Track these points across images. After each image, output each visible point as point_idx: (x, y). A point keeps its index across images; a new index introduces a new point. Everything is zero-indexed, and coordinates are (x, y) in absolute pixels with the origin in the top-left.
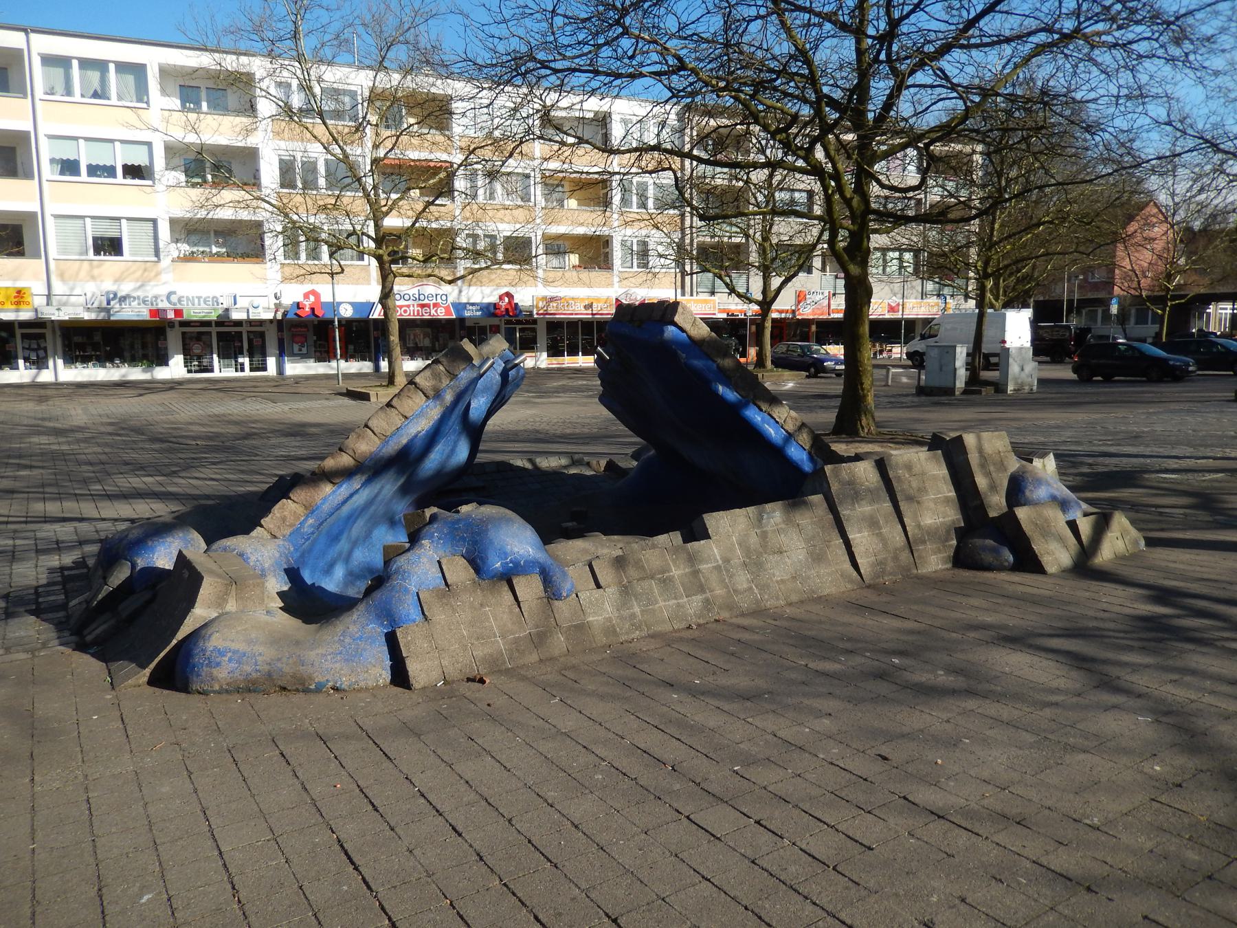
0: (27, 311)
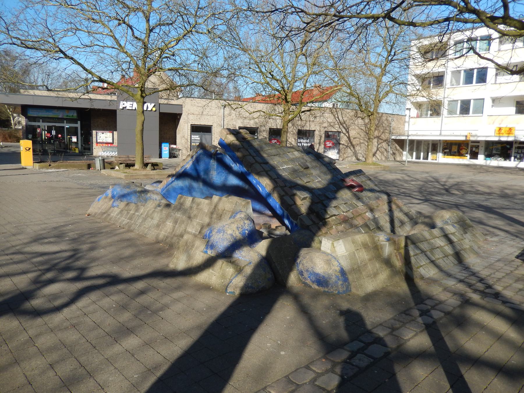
0: (512, 137)
